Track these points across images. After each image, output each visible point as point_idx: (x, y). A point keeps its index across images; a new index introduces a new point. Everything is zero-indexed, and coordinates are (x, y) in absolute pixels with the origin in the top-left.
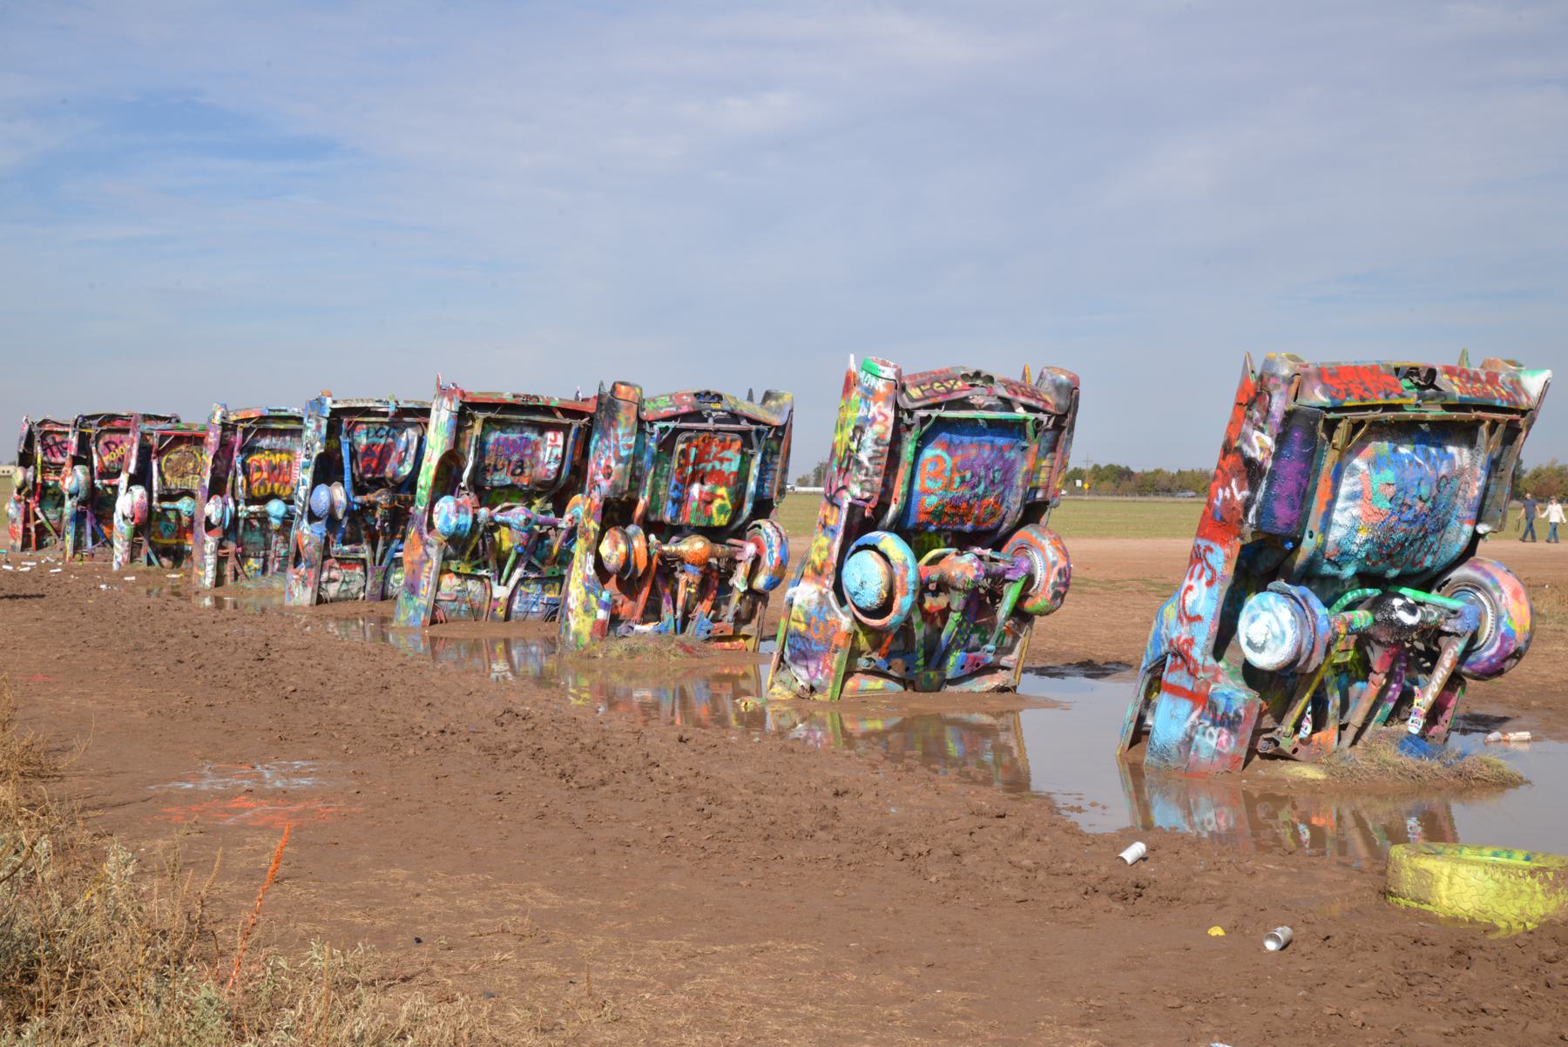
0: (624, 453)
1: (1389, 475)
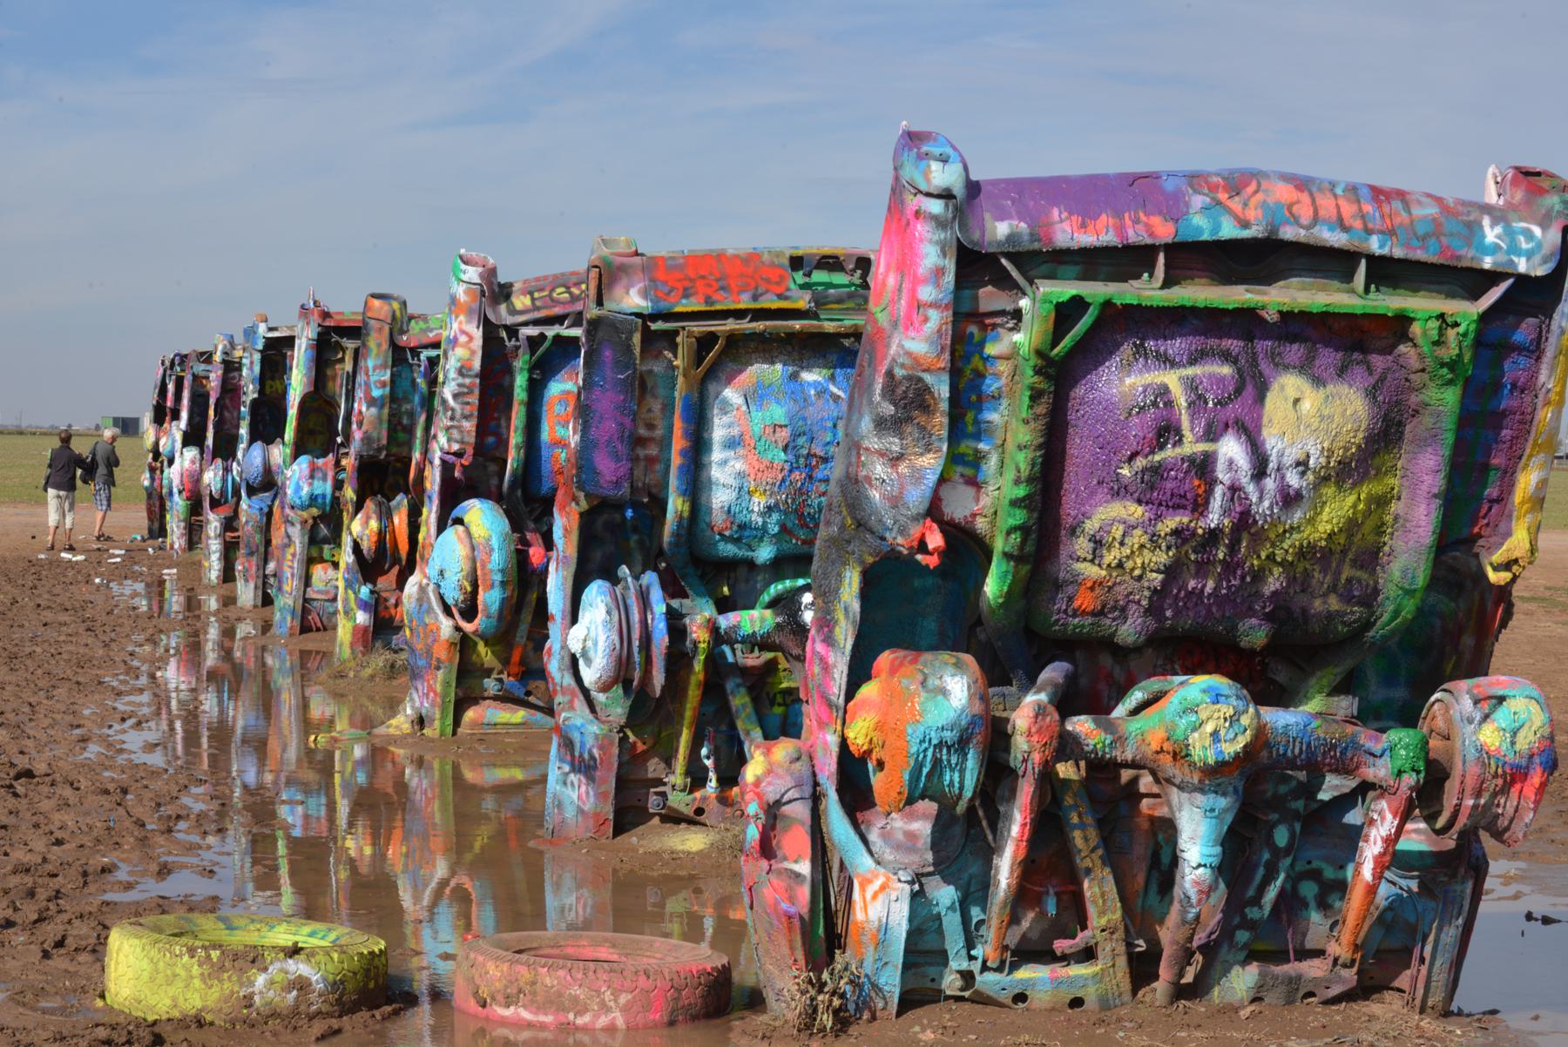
0: (376, 393)
1: (777, 412)
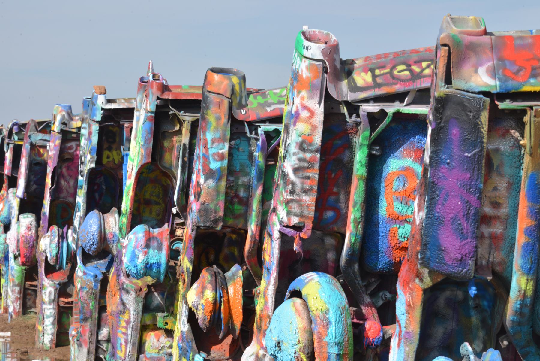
0: (214, 165)
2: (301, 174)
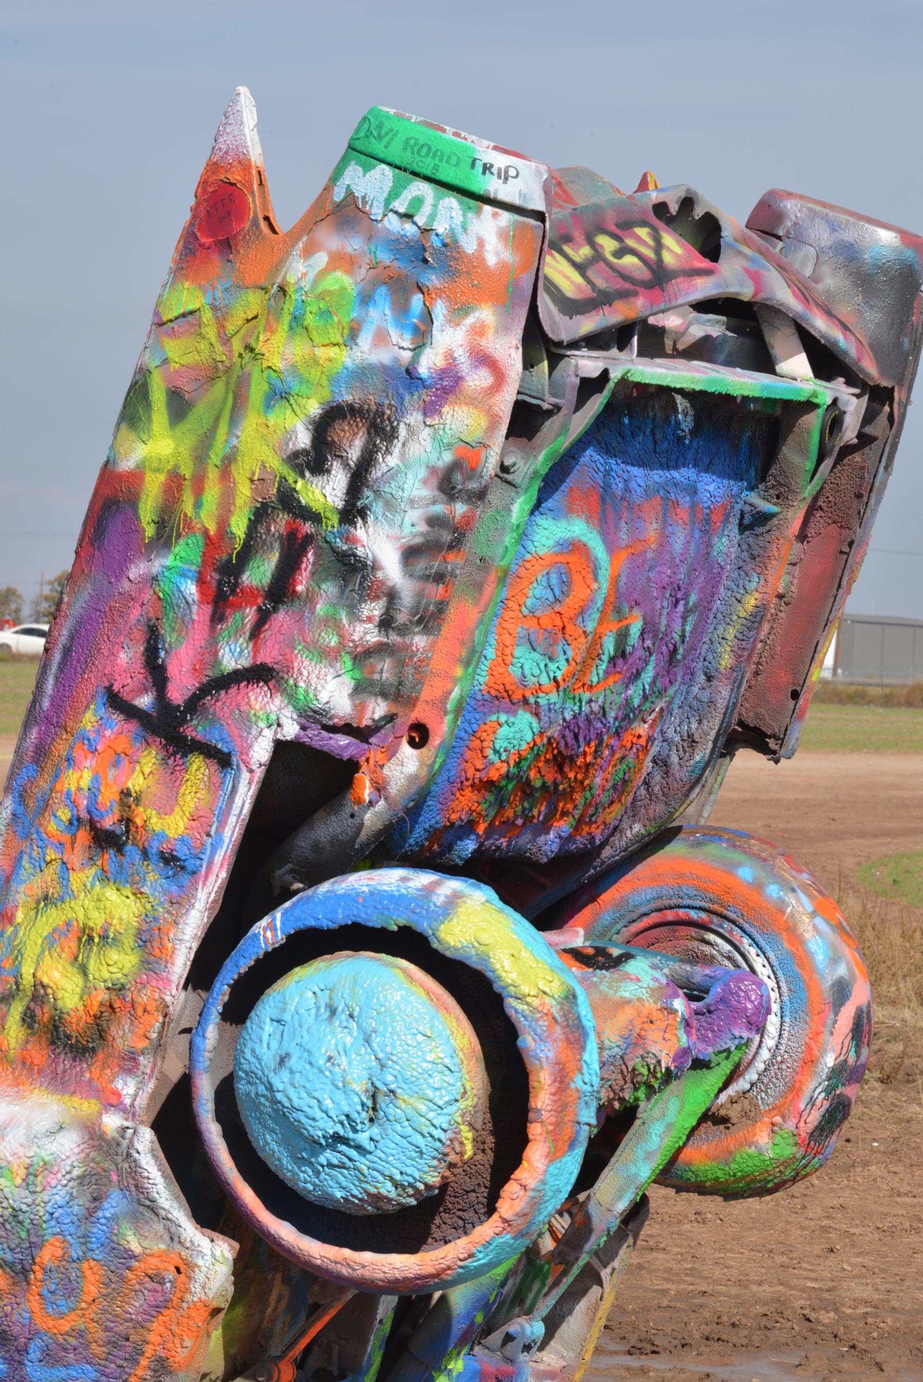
2: (421, 565)
